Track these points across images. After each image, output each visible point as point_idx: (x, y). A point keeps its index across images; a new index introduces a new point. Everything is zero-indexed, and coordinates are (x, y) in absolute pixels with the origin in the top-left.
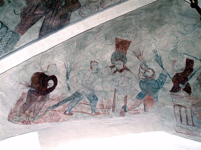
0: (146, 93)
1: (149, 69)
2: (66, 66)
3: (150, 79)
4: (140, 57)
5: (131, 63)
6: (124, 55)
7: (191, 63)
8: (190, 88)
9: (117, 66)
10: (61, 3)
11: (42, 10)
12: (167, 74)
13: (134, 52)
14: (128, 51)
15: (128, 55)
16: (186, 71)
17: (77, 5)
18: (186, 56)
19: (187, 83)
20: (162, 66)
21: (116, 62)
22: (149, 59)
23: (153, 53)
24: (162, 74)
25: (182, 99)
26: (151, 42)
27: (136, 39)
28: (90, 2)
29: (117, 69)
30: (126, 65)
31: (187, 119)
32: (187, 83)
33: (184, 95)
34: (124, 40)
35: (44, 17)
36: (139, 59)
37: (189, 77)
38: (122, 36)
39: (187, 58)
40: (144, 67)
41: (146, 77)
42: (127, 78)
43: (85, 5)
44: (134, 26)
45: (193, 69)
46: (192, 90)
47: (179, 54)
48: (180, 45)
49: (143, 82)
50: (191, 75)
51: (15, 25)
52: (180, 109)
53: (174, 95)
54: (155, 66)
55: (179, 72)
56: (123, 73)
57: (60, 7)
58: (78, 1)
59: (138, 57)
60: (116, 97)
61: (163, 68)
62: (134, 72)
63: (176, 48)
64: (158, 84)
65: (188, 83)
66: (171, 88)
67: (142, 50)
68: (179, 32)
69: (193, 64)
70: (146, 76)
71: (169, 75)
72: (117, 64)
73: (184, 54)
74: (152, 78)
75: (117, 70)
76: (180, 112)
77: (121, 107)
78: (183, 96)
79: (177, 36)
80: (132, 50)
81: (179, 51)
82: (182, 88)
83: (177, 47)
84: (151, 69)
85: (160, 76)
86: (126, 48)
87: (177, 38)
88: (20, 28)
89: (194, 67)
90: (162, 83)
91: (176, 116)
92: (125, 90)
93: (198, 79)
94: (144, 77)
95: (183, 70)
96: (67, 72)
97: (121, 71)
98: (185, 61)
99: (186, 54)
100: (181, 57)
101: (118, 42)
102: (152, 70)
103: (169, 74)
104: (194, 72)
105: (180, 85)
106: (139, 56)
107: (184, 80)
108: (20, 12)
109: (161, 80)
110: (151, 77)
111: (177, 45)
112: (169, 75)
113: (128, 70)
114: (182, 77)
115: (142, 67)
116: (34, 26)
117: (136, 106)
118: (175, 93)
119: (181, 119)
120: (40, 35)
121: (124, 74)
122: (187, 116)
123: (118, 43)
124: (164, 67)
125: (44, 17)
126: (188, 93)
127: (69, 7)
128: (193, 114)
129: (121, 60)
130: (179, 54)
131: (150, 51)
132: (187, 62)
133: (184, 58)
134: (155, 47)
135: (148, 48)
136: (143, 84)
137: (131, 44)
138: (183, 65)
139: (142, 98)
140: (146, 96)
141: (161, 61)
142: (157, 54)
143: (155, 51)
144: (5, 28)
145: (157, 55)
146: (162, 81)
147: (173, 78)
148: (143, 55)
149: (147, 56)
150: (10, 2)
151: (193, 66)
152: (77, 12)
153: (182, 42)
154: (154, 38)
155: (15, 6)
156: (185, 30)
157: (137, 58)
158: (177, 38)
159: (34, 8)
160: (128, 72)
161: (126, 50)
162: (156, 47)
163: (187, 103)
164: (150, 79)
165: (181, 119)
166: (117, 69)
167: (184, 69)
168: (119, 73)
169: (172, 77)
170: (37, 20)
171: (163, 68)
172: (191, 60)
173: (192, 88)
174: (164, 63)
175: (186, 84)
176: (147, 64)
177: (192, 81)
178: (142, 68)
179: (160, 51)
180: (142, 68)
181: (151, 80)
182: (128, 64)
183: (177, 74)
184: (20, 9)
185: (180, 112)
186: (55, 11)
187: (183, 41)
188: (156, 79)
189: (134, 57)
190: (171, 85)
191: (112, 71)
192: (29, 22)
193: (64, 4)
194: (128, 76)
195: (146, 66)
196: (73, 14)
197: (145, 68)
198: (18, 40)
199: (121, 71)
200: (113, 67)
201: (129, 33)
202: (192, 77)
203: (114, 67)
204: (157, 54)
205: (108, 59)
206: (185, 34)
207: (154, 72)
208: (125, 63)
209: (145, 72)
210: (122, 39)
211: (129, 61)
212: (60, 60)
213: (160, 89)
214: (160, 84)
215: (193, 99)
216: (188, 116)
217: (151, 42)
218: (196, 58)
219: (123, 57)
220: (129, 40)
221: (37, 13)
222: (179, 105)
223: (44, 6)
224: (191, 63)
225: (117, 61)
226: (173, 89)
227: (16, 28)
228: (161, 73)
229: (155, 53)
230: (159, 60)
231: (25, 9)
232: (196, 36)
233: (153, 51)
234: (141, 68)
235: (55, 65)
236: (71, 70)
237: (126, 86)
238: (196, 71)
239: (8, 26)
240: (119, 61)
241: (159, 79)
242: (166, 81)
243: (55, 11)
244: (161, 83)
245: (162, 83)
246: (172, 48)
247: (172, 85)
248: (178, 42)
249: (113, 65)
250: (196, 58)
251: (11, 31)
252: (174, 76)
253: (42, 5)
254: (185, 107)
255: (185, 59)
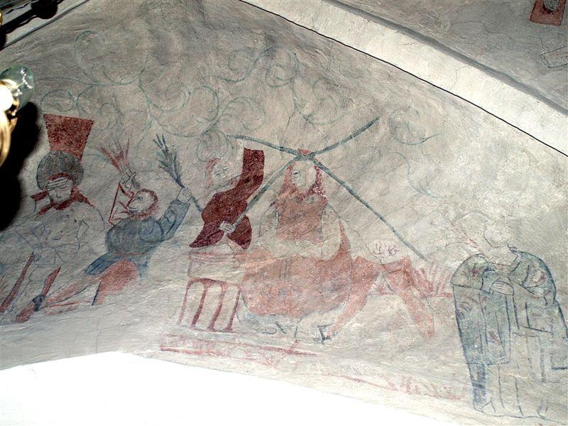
0: (116, 258)
1: (143, 190)
3: (142, 219)
4: (121, 163)
5: (94, 182)
6: (76, 160)
7: (258, 161)
8: (249, 231)
9: (52, 193)
12: (191, 200)
13: (104, 150)
14: (85, 150)
15: (86, 162)
16: (242, 184)
18: (243, 144)
19: (242, 217)
20: (178, 181)
21: (52, 183)
22: (145, 164)
23: (155, 145)
24: (177, 201)
25: (220, 263)
26: (148, 114)
27: (104, 113)
29: (52, 200)
30: (79, 187)
31: (217, 316)
32: (242, 217)
33: (228, 250)
34: (71, 118)
36: (118, 168)
37: (248, 201)
38: (59, 107)
39: (245, 149)
40: (130, 185)
41: (131, 213)
42: (76, 221)
44: (86, 74)
45: (262, 176)
46: (254, 235)
47: (223, 138)
48: (226, 114)
49: (119, 227)
50: (256, 193)
52: (205, 291)
53: (198, 253)
54: (159, 183)
55: (223, 190)
56: (67, 210)
59: (114, 164)
60: (29, 273)
61: (181, 185)
62: (97, 205)
63: (215, 124)
64: (162, 231)
65: (246, 218)
66: (194, 236)
67: (126, 142)
68: (218, 77)
69: (263, 161)
70: (132, 212)
71: (196, 201)
72: (54, 188)
73: (237, 137)
74: (146, 215)
75: (53, 204)
76: (203, 298)
77: (31, 299)
78: (226, 254)
79: (214, 88)
80: (98, 146)
81: (223, 130)
82: (225, 234)
83: (218, 121)
84: (147, 191)
85: (169, 207)
86: (80, 142)
87: (216, 94)
89: (266, 171)
90: (174, 226)
91: (183, 309)
92: (61, 254)
93: (274, 203)
94: (126, 216)
95: (234, 183)
97: (63, 205)
98: (240, 157)
99: (242, 137)
100: (230, 146)
101: (55, 125)
102: (152, 193)
103: (197, 198)
104: (264, 186)
105: (223, 226)
106: (117, 159)
107: (236, 209)
109: (172, 219)
110: (145, 212)
111: (218, 116)
112: (196, 201)
113: (82, 199)
114: (230, 204)
115: (124, 189)
117: (73, 293)
118: (202, 250)
119: (197, 317)
121: (70, 214)
122: (220, 307)
123: (53, 128)
124: (184, 181)
126: (240, 245)
128: (241, 301)
129: (67, 175)
130: (223, 138)
131: (149, 144)
132: (245, 161)
133: (238, 147)
134: (160, 128)
135: (143, 135)
136: (117, 233)
137: (93, 127)
138: (233, 168)
139: (101, 272)
140: (114, 264)
141: (175, 166)
142: (166, 147)
143: (162, 141)
145: (166, 151)
146: (176, 220)
147: (205, 209)
148: (130, 155)
149: (140, 155)
151: (262, 168)
153: (230, 105)
154: (154, 105)
156: (231, 69)
157: (112, 167)
158: (216, 94)
160: (83, 206)
161: (80, 146)
162: (164, 129)
163: (234, 271)
164: (142, 219)
165: (197, 317)
166: (52, 200)
167: (236, 180)
168: (56, 211)
169: (203, 207)
171: (181, 185)
172: (256, 152)
173: (255, 229)
174: (183, 170)
175: (239, 220)
176: (139, 179)
177: (257, 211)
178: (123, 192)
179: (174, 138)
180: (123, 192)
181: (145, 221)
182: (85, 186)
183: (217, 197)
185: (203, 298)
187: (231, 102)
188: (159, 215)
189: (105, 163)
190: (198, 227)
191: (37, 208)
194: (79, 217)
195: (136, 183)
197: (133, 189)
199: (63, 205)
200: (42, 198)
201: (79, 96)
202: (257, 200)
203: (45, 196)
204: (166, 147)
205: (29, 177)
206: (235, 82)
207: (156, 198)
208: (78, 184)
209: (129, 202)
210: (63, 115)
211: (89, 176)
213: (163, 243)
214: (168, 227)
215: (252, 260)
216: (223, 308)
217: (149, 117)
218: (270, 145)
219: (72, 167)
220: (84, 117)
222: (205, 279)
224: (258, 161)
225: (54, 179)
226: (199, 238)
228: (175, 197)
229: (160, 145)
230: (169, 163)
232: (262, 82)
233: (154, 140)
234: (120, 192)
237: (65, 245)
238: (271, 182)
240: (59, 179)
241: (167, 216)
242: (185, 219)
244: (171, 225)
245: (173, 225)
246: (203, 128)
247: (201, 228)
248: (219, 106)
249: (41, 191)
250: (270, 145)
252: (210, 204)
254: (222, 284)
255: (241, 151)
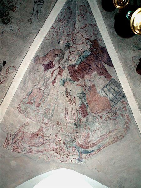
2: (135, 50)
10: (94, 51)
11: (98, 63)
17: (95, 41)
28: (94, 33)
35: (102, 62)
43: (96, 36)
51: (106, 80)
57: (97, 52)
58: (1, 124)
88: (108, 77)
96: (139, 50)
108: (99, 76)
116: (107, 69)
120: (112, 67)
125: (102, 62)
127: (97, 46)
144: (107, 86)
150: (93, 81)
152: (100, 42)
155: (96, 78)
159: (97, 67)
170: (104, 66)
184: (97, 76)
186: (99, 55)
192: (105, 72)
193: (95, 49)
196: (101, 45)
198: (114, 80)
212: (130, 54)
215: (45, 138)
221: (100, 66)
223: (96, 62)
227: (108, 80)
231: (97, 73)
235: (133, 57)
236: (138, 46)
239: (106, 84)
243: (99, 55)
251: (109, 83)
253: (96, 63)
